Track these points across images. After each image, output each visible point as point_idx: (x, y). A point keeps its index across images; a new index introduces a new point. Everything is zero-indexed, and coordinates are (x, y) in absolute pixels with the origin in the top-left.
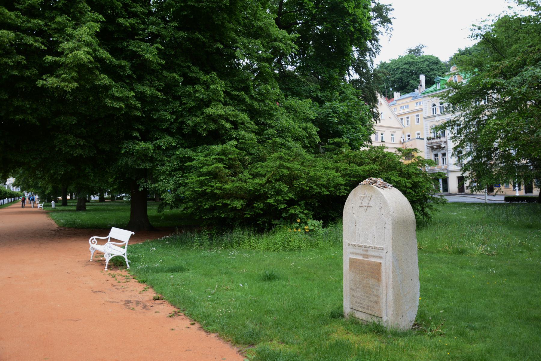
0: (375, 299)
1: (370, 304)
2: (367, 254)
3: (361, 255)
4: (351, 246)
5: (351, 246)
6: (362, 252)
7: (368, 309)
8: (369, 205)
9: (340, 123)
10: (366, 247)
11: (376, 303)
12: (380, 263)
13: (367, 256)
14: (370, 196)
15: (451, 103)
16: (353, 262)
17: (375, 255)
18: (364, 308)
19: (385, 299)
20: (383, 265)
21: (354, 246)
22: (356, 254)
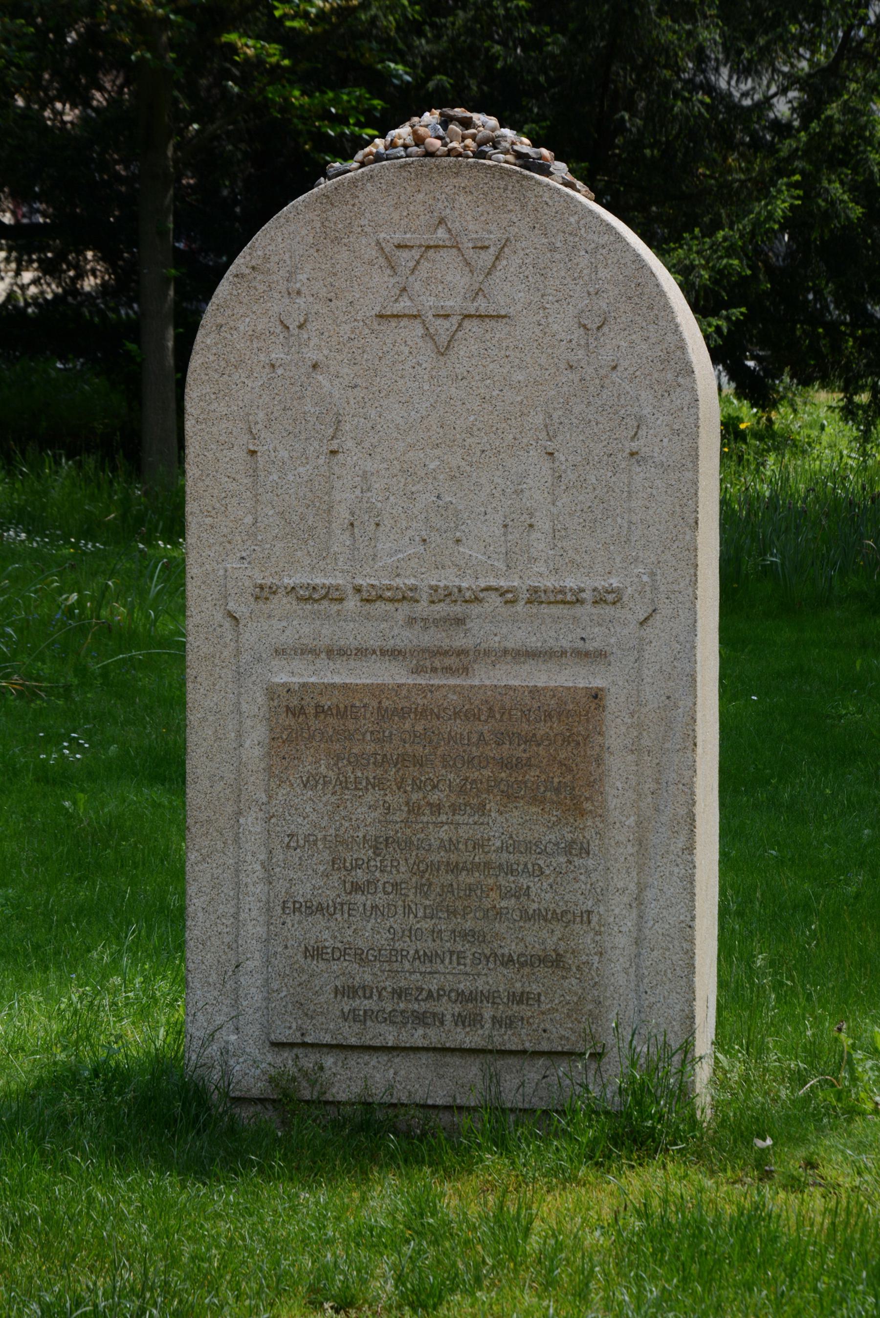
0: (540, 938)
1: (496, 979)
2: (460, 641)
3: (394, 654)
4: (282, 603)
5: (282, 603)
6: (407, 638)
7: (470, 1021)
8: (482, 305)
9: (747, 171)
10: (449, 595)
11: (556, 961)
12: (596, 696)
13: (462, 660)
14: (495, 236)
15: (152, 1074)
16: (303, 721)
17: (534, 642)
18: (421, 1019)
19: (629, 924)
20: (616, 732)
21: (309, 596)
22: (334, 653)
